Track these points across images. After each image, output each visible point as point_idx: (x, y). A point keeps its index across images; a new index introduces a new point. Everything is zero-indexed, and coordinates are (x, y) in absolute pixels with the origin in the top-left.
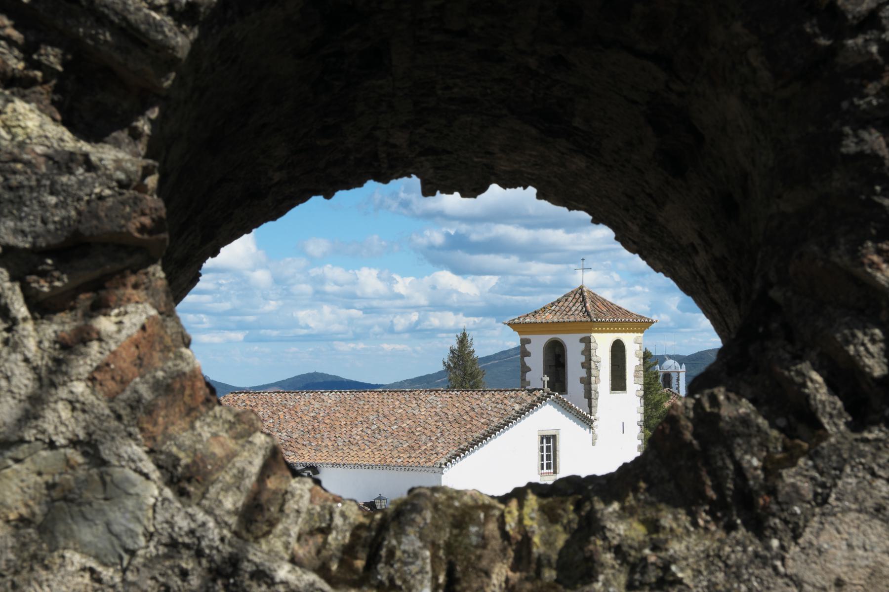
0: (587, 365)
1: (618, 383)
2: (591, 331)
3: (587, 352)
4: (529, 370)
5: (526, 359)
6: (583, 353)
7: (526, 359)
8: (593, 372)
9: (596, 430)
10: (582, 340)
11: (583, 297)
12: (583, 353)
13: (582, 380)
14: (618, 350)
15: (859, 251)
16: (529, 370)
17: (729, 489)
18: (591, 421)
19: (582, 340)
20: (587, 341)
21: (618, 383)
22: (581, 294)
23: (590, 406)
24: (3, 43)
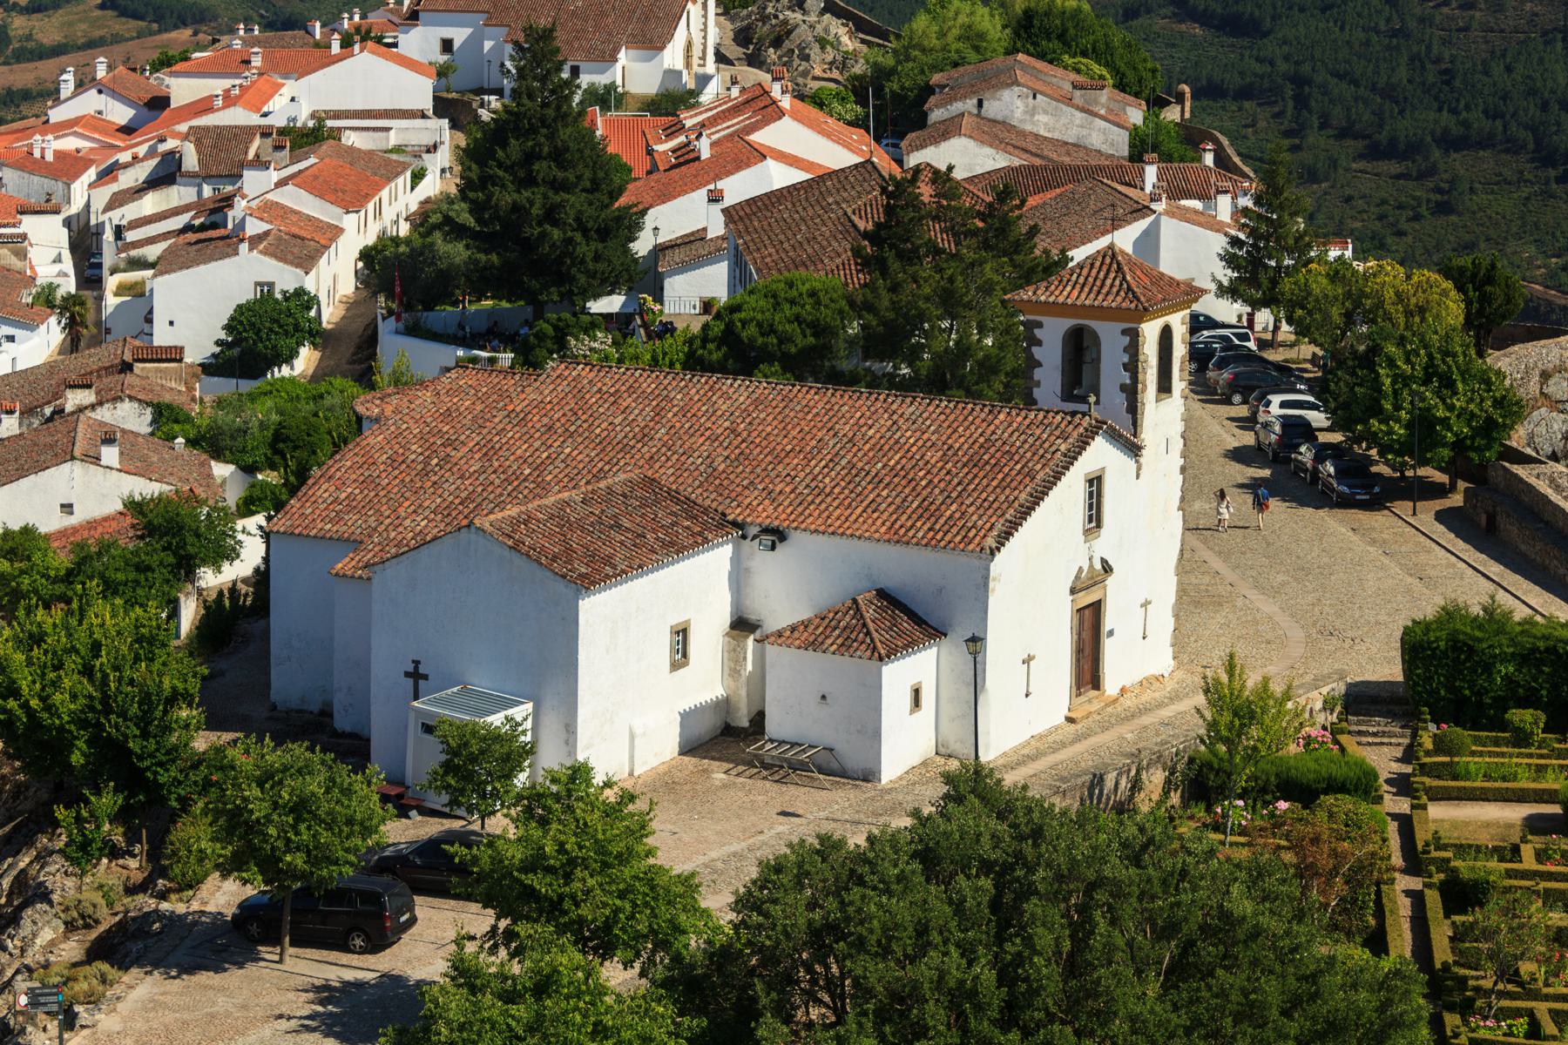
0: (1133, 367)
1: (1165, 387)
2: (1141, 321)
3: (1133, 349)
4: (1040, 365)
5: (1035, 349)
6: (1125, 350)
7: (1035, 349)
8: (1140, 377)
9: (1142, 460)
10: (1124, 332)
11: (1119, 264)
12: (1125, 350)
13: (1123, 388)
14: (1166, 334)
15: (116, 790)
16: (1040, 365)
17: (896, 367)
18: (1140, 448)
19: (1124, 332)
20: (1134, 336)
21: (1165, 387)
22: (1114, 256)
23: (1135, 424)
24: (1567, 489)
